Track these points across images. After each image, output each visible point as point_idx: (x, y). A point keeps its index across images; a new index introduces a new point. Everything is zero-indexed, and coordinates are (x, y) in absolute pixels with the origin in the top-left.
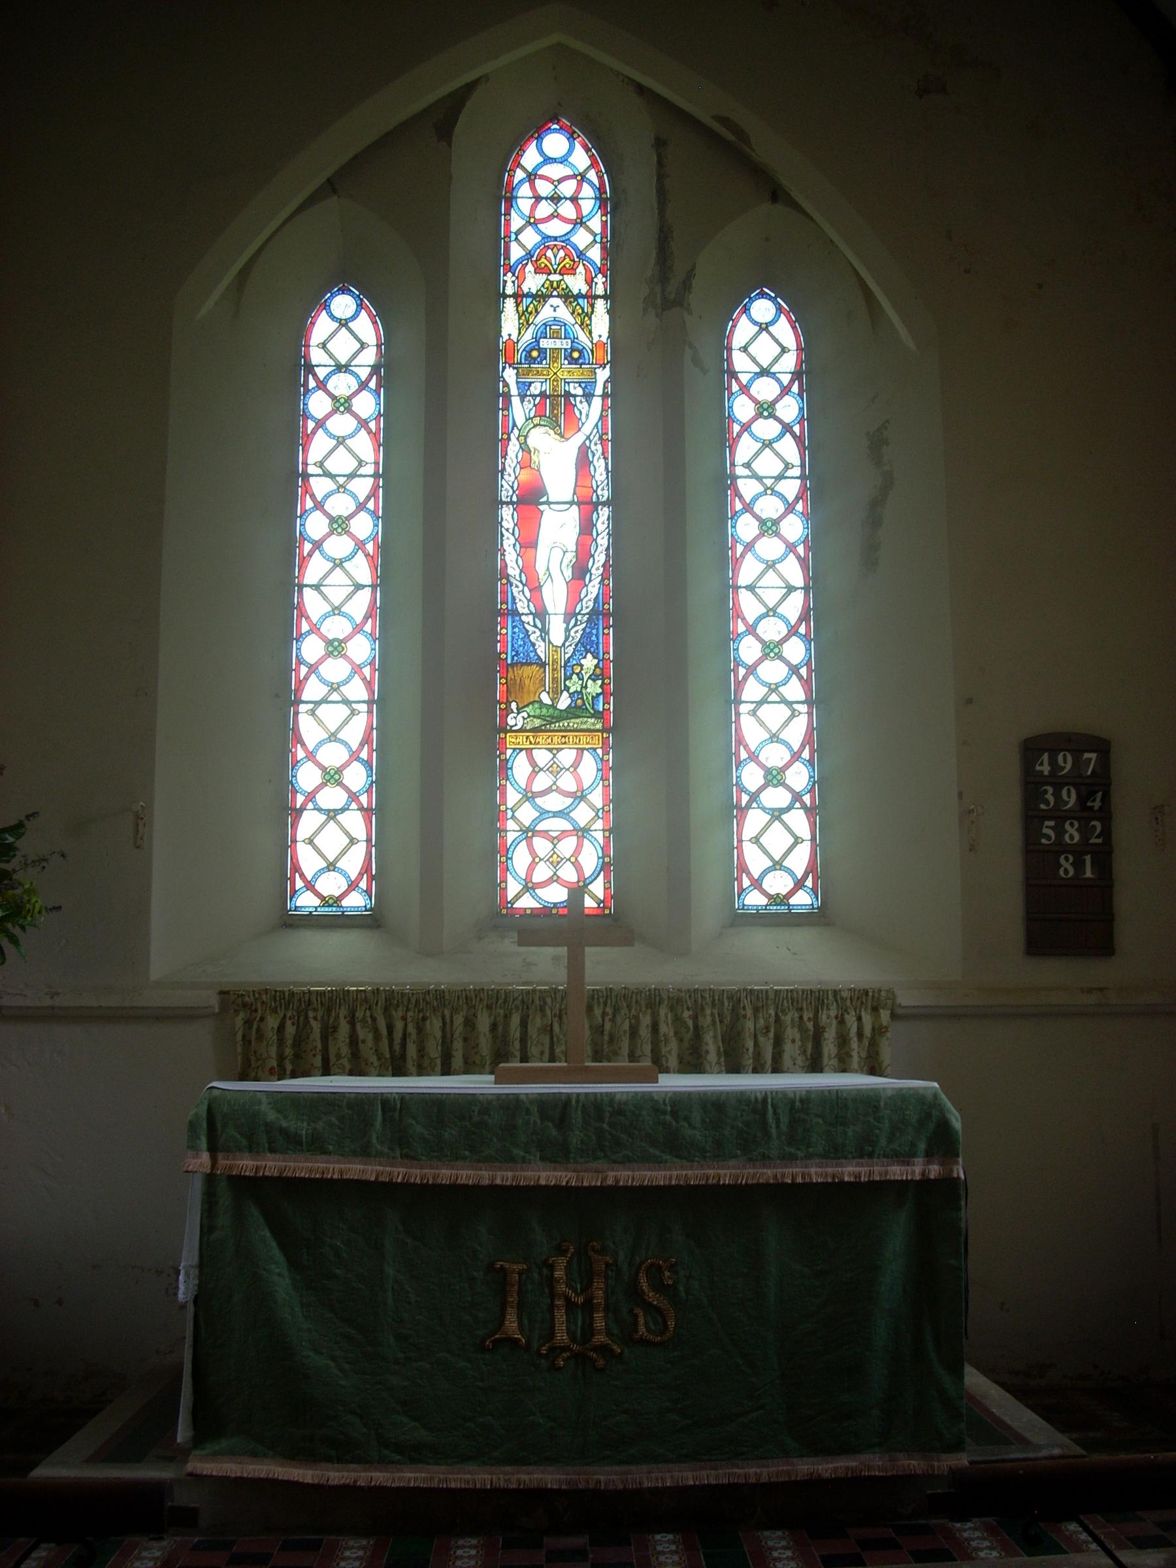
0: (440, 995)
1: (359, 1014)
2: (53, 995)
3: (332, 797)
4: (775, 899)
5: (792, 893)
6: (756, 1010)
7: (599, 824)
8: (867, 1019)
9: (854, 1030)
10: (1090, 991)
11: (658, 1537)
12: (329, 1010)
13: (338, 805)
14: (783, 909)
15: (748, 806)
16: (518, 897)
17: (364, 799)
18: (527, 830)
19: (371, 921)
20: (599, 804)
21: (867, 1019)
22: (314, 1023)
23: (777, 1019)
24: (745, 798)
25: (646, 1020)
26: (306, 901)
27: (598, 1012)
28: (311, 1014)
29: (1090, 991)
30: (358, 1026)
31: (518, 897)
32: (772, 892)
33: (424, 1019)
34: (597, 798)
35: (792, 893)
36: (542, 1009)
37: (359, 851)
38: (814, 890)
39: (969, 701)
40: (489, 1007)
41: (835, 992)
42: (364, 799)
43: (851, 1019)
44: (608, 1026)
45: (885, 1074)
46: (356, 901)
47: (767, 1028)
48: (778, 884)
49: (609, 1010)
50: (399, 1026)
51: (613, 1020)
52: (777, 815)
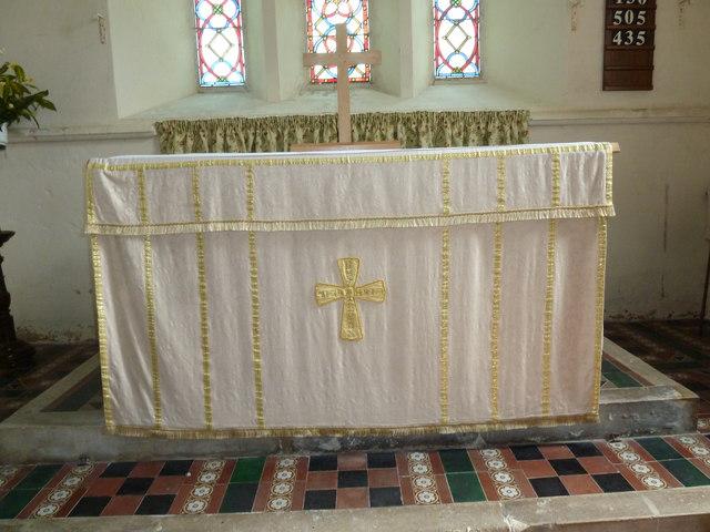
0: (275, 120)
1: (228, 132)
2: (64, 129)
3: (218, 21)
4: (455, 70)
5: (465, 66)
6: (453, 124)
7: (362, 32)
8: (516, 129)
9: (508, 135)
10: (637, 110)
11: (413, 456)
12: (212, 131)
13: (223, 26)
14: (460, 75)
15: (442, 19)
16: (320, 73)
17: (235, 21)
18: (324, 36)
19: (246, 89)
20: (361, 21)
21: (516, 129)
22: (204, 139)
23: (466, 129)
24: (440, 15)
25: (391, 131)
26: (209, 80)
27: (363, 127)
28: (201, 134)
29: (637, 110)
30: (228, 138)
31: (320, 73)
32: (454, 66)
33: (266, 134)
34: (360, 17)
35: (465, 66)
36: (331, 126)
37: (236, 49)
38: (477, 64)
39: (234, 434)
40: (302, 126)
41: (498, 113)
42: (235, 21)
43: (507, 128)
44: (368, 134)
45: (94, 337)
46: (236, 79)
47: (460, 134)
48: (458, 61)
49: (369, 126)
50: (251, 138)
51: (371, 131)
52: (457, 23)
